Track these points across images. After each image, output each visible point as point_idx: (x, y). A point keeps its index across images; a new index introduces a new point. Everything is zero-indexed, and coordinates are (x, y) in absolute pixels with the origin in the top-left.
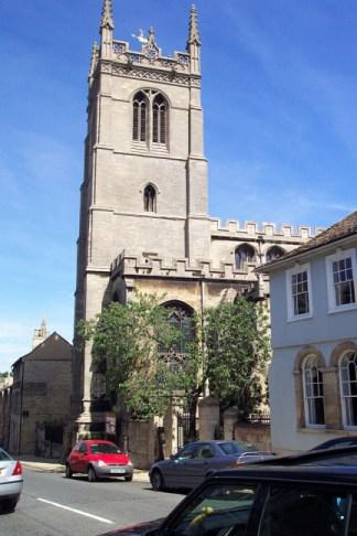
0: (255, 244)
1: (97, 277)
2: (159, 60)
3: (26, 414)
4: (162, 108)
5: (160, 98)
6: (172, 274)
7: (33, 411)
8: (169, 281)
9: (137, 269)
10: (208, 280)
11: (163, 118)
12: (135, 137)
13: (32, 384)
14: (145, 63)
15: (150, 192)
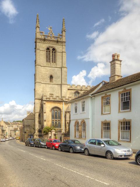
0: (80, 91)
1: (38, 100)
2: (53, 37)
3: (25, 132)
4: (55, 52)
5: (54, 49)
7: (27, 132)
10: (65, 101)
12: (47, 61)
13: (27, 126)
14: (49, 38)
15: (51, 77)
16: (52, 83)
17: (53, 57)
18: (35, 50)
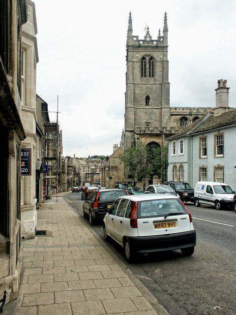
4: (153, 62)
5: (152, 58)
6: (152, 132)
7: (113, 177)
8: (151, 135)
9: (140, 131)
11: (153, 66)
12: (142, 76)
13: (112, 167)
15: (148, 98)
16: (148, 107)
17: (150, 69)
18: (136, 117)
